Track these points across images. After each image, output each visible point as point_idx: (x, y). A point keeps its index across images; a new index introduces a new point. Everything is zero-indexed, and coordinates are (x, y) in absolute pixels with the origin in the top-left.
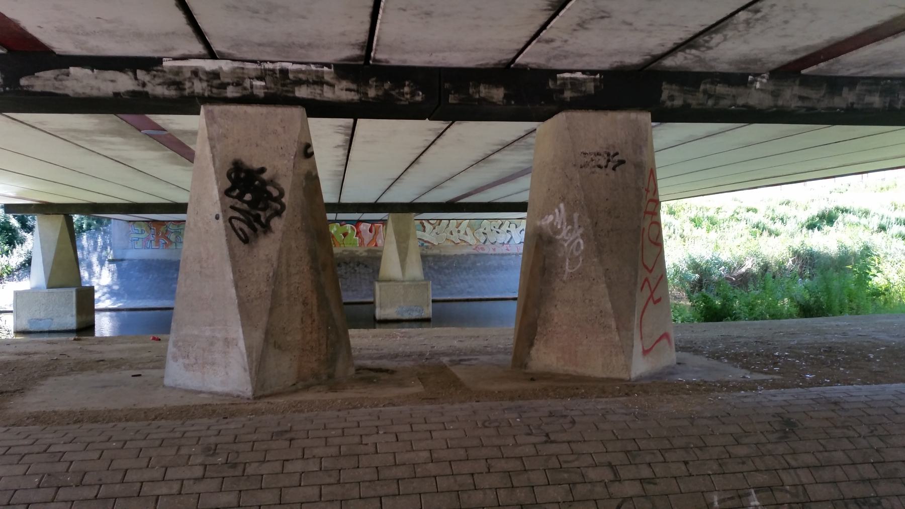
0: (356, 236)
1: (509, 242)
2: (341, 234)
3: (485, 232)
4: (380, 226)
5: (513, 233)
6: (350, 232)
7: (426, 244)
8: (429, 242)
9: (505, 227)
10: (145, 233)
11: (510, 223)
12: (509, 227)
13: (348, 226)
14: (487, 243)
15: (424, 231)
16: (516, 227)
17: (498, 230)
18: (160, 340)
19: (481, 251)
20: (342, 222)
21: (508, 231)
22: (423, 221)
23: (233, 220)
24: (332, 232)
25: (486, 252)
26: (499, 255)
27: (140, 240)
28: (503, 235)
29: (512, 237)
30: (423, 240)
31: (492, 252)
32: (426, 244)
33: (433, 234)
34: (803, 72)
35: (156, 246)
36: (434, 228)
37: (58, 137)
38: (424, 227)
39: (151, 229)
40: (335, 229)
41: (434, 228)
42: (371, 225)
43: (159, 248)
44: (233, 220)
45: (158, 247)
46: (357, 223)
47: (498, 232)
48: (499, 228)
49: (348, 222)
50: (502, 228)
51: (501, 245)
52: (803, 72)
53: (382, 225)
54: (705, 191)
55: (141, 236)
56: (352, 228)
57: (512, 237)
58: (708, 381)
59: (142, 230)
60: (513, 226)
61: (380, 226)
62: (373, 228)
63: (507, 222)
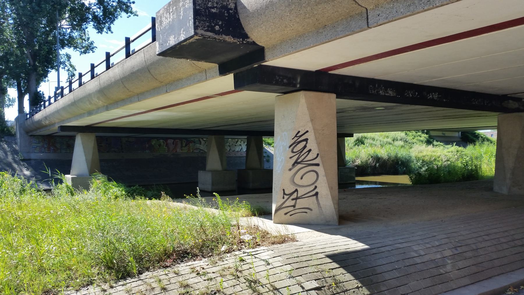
0: (165, 147)
1: (240, 150)
2: (158, 145)
3: (230, 145)
4: (178, 141)
5: (242, 146)
6: (162, 144)
7: (201, 151)
8: (203, 151)
9: (239, 143)
10: (41, 143)
11: (241, 141)
12: (241, 143)
13: (161, 141)
14: (231, 151)
15: (200, 144)
16: (244, 143)
17: (236, 144)
18: (371, 237)
19: (229, 155)
20: (158, 139)
21: (240, 145)
22: (200, 139)
23: (294, 151)
24: (153, 144)
25: (232, 155)
26: (238, 157)
27: (38, 147)
28: (238, 147)
29: (242, 148)
30: (200, 149)
31: (234, 156)
32: (201, 151)
33: (205, 146)
34: (330, 72)
35: (48, 151)
36: (205, 143)
37: (77, 88)
38: (200, 142)
39: (45, 140)
40: (154, 142)
41: (205, 143)
42: (173, 140)
43: (50, 153)
44: (294, 151)
45: (49, 152)
46: (166, 139)
47: (236, 145)
48: (236, 143)
49: (162, 138)
50: (238, 143)
51: (237, 152)
52: (330, 72)
53: (179, 140)
54: (388, 131)
55: (38, 145)
56: (163, 142)
57: (242, 148)
58: (214, 208)
59: (39, 141)
60: (242, 142)
61: (178, 141)
62: (175, 142)
63: (240, 140)
